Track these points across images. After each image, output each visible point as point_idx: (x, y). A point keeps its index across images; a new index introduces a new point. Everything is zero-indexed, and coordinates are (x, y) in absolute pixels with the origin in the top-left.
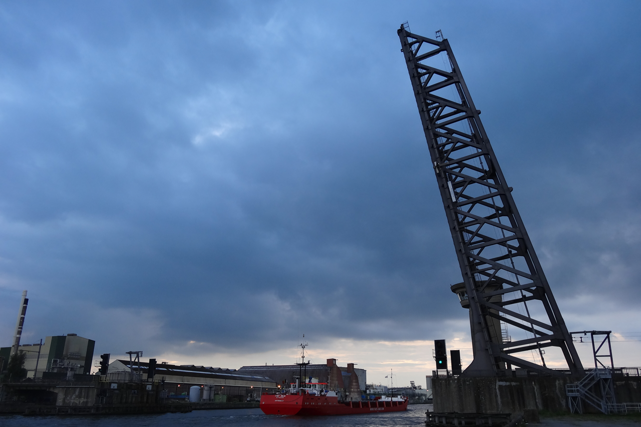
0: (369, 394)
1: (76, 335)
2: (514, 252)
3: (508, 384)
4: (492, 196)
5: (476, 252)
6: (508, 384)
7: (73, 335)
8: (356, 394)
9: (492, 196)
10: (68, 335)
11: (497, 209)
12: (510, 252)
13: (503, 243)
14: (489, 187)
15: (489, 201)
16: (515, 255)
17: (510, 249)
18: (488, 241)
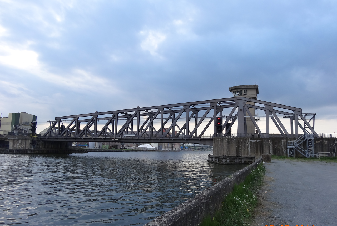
0: (185, 146)
1: (26, 113)
2: (195, 115)
3: (255, 141)
5: (189, 133)
6: (255, 141)
7: (24, 113)
8: (178, 146)
10: (21, 113)
12: (194, 117)
13: (189, 119)
14: (179, 118)
16: (197, 115)
17: (193, 117)
18: (186, 126)
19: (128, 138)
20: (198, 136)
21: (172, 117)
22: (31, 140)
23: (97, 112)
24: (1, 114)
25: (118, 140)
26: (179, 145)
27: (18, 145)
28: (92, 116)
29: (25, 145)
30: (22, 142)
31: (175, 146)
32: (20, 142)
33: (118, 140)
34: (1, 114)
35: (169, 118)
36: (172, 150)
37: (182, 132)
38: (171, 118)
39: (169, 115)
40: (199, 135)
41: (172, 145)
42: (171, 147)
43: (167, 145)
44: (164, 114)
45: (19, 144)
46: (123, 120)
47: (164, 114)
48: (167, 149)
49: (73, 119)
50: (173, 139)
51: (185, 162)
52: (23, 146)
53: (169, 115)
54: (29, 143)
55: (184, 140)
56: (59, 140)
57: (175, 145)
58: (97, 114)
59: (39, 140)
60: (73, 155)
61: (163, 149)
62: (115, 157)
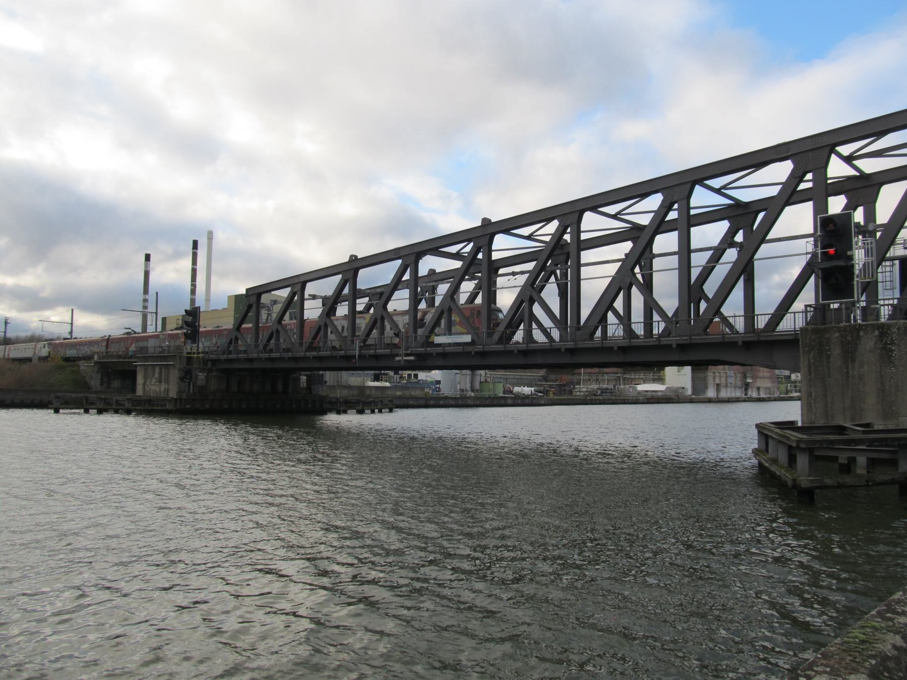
4: (685, 251)
8: (767, 381)
9: (685, 251)
11: (728, 241)
15: (699, 260)
19: (448, 349)
20: (761, 323)
21: (739, 237)
22: (179, 369)
23: (353, 259)
24: (157, 293)
25: (412, 358)
26: (770, 378)
27: (153, 383)
28: (340, 276)
29: (168, 383)
30: (160, 374)
31: (755, 382)
32: (157, 375)
33: (412, 358)
34: (157, 293)
35: (723, 247)
36: (746, 394)
37: (616, 313)
38: (733, 244)
39: (723, 226)
40: (767, 318)
41: (745, 377)
42: (739, 383)
43: (723, 380)
44: (693, 230)
45: (154, 380)
46: (514, 274)
47: (693, 230)
48: (724, 394)
49: (289, 289)
50: (566, 349)
51: (329, 423)
52: (163, 386)
53: (723, 226)
54: (175, 375)
55: (668, 347)
56: (256, 365)
57: (754, 377)
58: (356, 265)
59: (209, 365)
60: (332, 419)
61: (711, 393)
62: (498, 433)
